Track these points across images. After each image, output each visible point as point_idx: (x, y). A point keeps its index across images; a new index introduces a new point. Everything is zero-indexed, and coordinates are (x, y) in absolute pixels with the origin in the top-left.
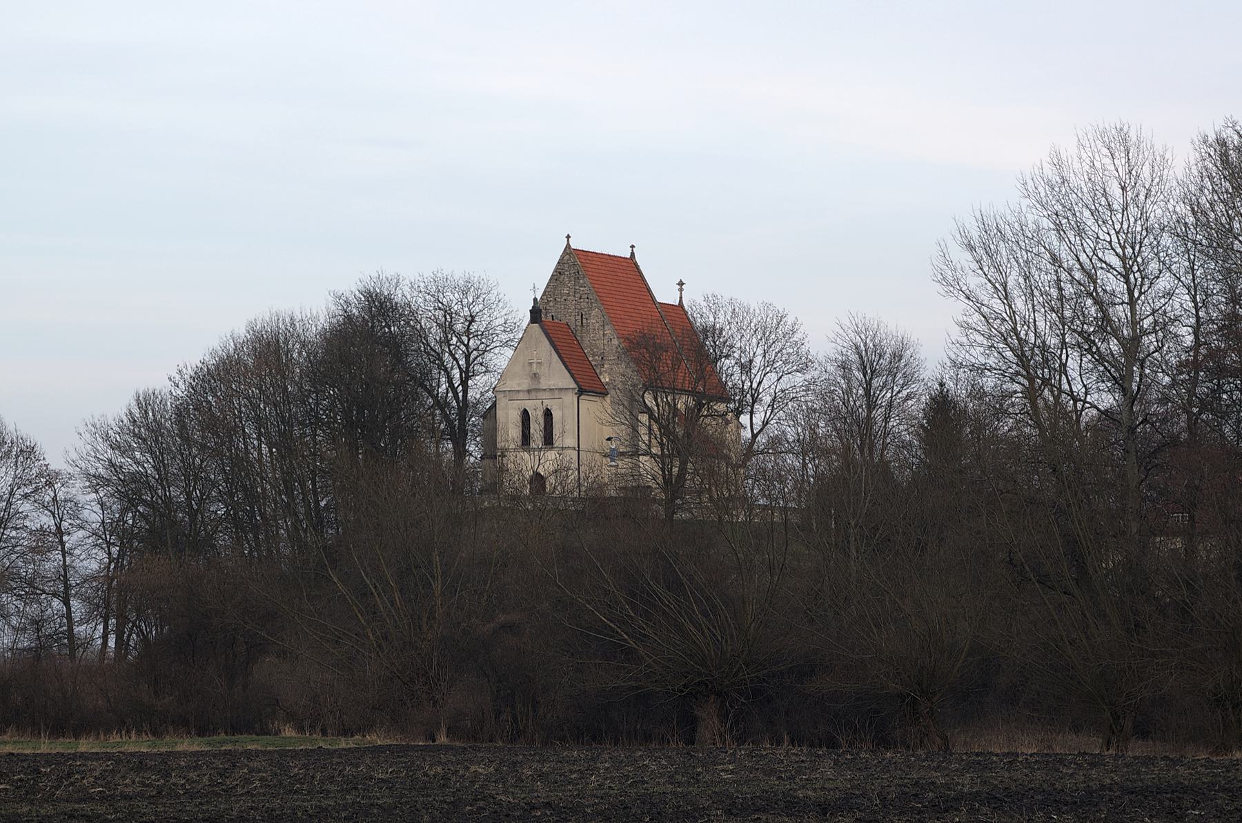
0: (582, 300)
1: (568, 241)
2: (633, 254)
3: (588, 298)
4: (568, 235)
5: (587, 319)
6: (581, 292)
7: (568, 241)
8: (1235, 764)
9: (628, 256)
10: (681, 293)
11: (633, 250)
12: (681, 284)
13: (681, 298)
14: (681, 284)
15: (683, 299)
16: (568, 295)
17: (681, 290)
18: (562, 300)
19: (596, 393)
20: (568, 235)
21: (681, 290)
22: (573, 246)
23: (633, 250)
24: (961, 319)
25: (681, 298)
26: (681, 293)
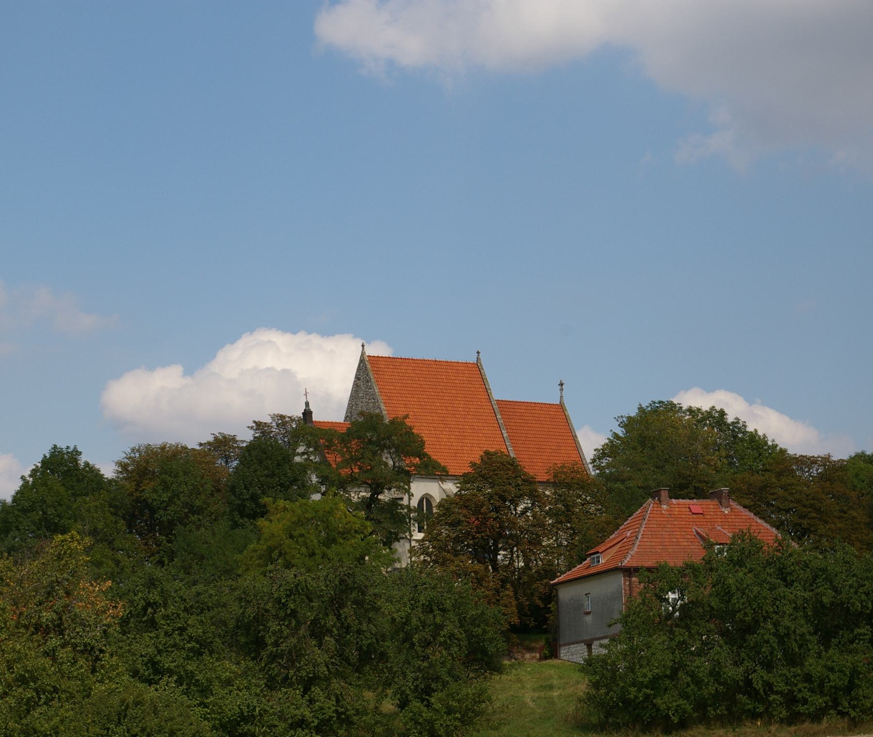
1: (363, 349)
7: (363, 349)
14: (561, 384)
17: (562, 390)
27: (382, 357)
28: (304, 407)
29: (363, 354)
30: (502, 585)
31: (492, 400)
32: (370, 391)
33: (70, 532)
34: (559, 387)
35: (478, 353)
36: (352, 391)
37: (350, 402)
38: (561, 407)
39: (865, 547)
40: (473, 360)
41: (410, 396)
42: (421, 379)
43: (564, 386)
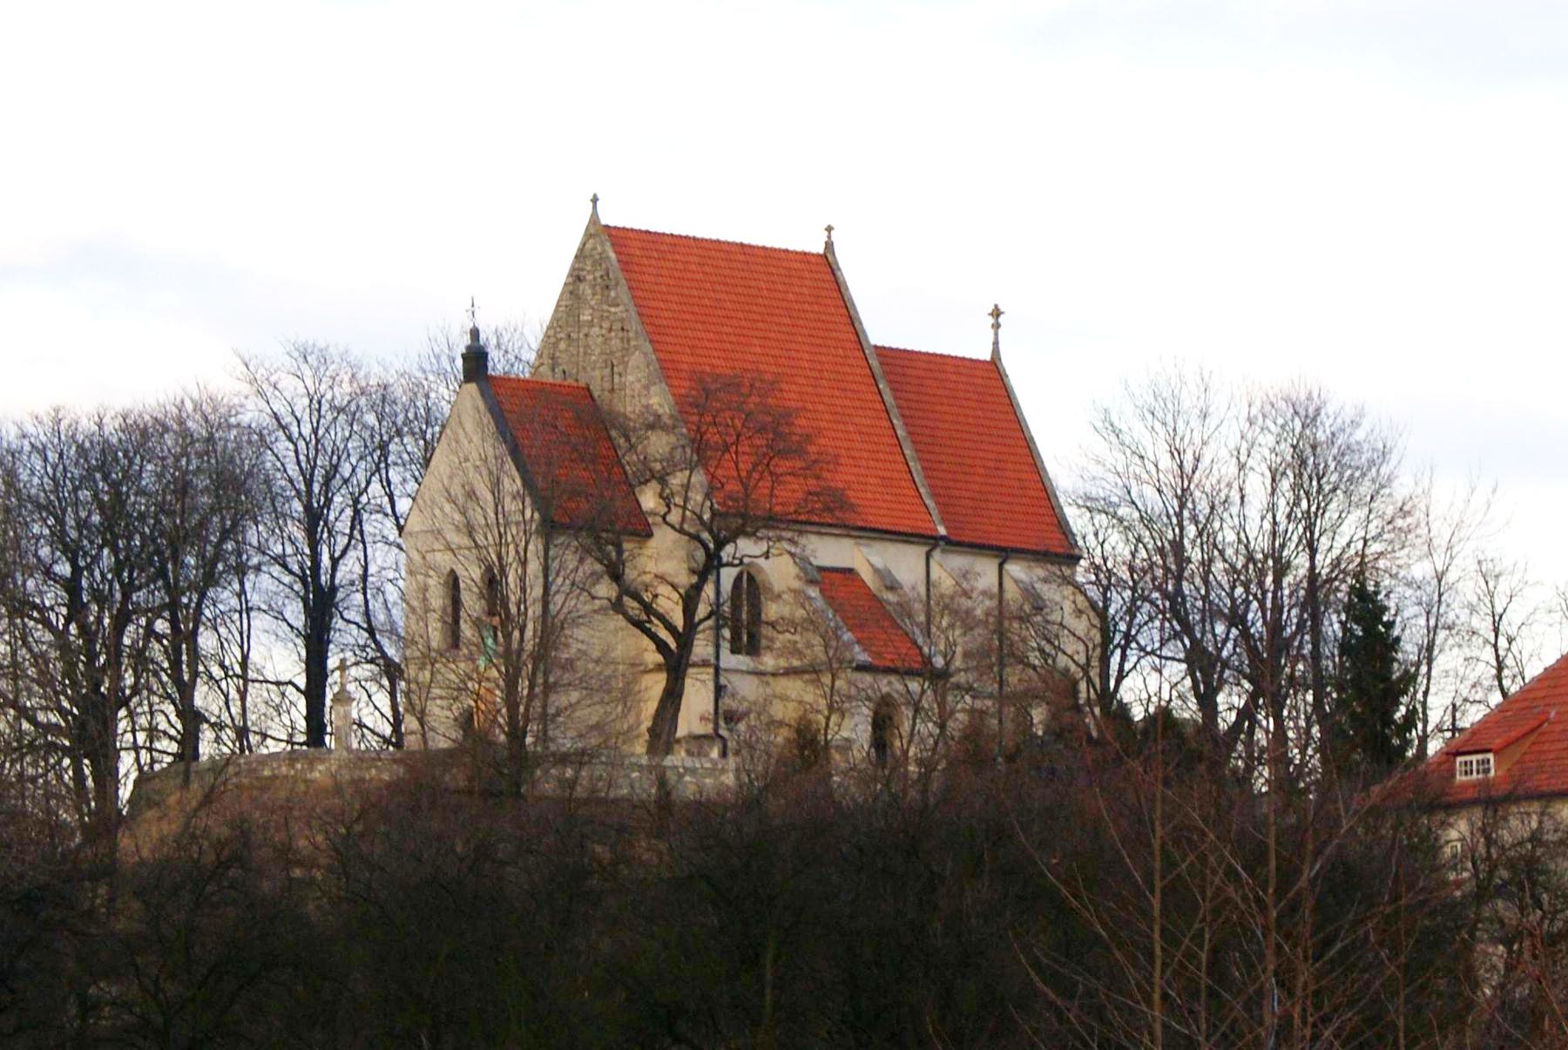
0: (613, 334)
1: (595, 207)
2: (829, 245)
3: (623, 329)
4: (595, 196)
5: (620, 375)
6: (612, 318)
7: (595, 207)
8: (1385, 1047)
9: (821, 250)
10: (996, 334)
11: (829, 237)
12: (996, 313)
13: (996, 343)
14: (996, 313)
15: (1001, 346)
16: (591, 324)
17: (997, 326)
18: (581, 336)
19: (846, 527)
20: (595, 196)
21: (997, 326)
22: (604, 220)
23: (829, 237)
24: (500, 328)
25: (996, 343)
26: (996, 334)
27: (632, 230)
28: (467, 340)
29: (594, 219)
30: (79, 735)
31: (865, 346)
32: (613, 310)
33: (359, 750)
34: (991, 320)
35: (829, 229)
36: (558, 306)
37: (551, 333)
38: (992, 371)
39: (1436, 802)
40: (819, 248)
41: (699, 326)
42: (718, 287)
43: (1001, 319)
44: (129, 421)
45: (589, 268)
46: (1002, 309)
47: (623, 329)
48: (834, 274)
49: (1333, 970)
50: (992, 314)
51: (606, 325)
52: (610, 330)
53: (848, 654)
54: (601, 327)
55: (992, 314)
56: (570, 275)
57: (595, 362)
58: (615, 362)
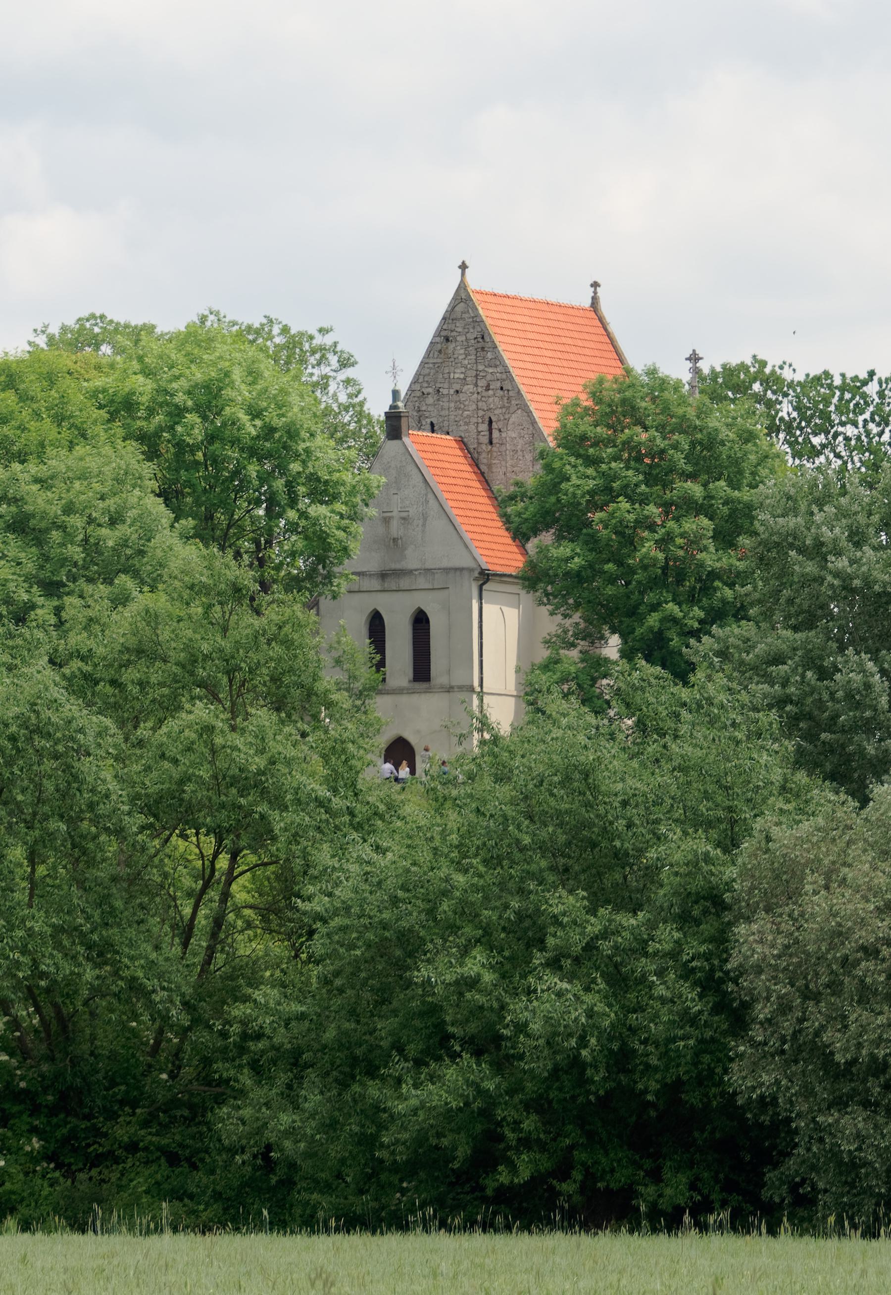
0: (491, 392)
4: (463, 263)
11: (595, 293)
20: (463, 263)
23: (595, 293)
29: (462, 286)
32: (490, 370)
37: (417, 387)
44: (158, 491)
45: (460, 330)
46: (467, 263)
47: (502, 388)
48: (606, 330)
49: (99, 1156)
50: (689, 359)
51: (482, 383)
52: (488, 388)
53: (876, 587)
54: (476, 385)
55: (689, 359)
56: (438, 334)
57: (469, 417)
58: (493, 419)
